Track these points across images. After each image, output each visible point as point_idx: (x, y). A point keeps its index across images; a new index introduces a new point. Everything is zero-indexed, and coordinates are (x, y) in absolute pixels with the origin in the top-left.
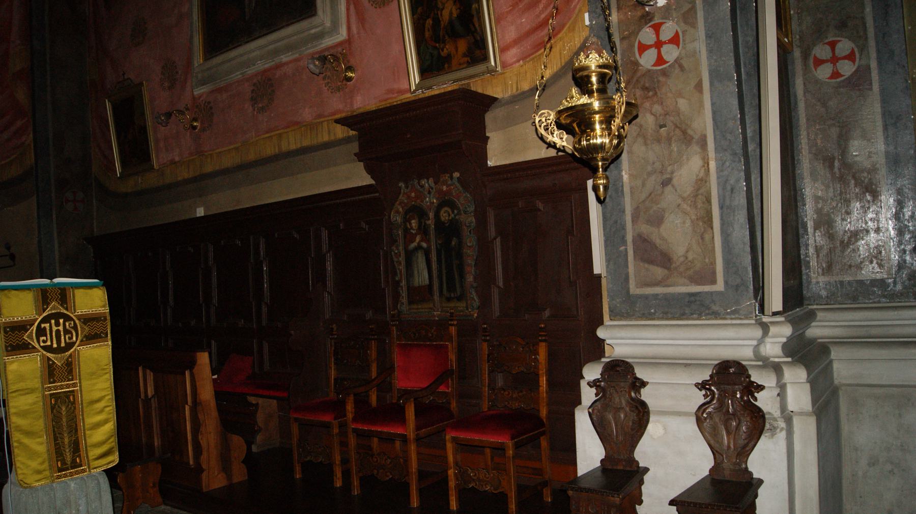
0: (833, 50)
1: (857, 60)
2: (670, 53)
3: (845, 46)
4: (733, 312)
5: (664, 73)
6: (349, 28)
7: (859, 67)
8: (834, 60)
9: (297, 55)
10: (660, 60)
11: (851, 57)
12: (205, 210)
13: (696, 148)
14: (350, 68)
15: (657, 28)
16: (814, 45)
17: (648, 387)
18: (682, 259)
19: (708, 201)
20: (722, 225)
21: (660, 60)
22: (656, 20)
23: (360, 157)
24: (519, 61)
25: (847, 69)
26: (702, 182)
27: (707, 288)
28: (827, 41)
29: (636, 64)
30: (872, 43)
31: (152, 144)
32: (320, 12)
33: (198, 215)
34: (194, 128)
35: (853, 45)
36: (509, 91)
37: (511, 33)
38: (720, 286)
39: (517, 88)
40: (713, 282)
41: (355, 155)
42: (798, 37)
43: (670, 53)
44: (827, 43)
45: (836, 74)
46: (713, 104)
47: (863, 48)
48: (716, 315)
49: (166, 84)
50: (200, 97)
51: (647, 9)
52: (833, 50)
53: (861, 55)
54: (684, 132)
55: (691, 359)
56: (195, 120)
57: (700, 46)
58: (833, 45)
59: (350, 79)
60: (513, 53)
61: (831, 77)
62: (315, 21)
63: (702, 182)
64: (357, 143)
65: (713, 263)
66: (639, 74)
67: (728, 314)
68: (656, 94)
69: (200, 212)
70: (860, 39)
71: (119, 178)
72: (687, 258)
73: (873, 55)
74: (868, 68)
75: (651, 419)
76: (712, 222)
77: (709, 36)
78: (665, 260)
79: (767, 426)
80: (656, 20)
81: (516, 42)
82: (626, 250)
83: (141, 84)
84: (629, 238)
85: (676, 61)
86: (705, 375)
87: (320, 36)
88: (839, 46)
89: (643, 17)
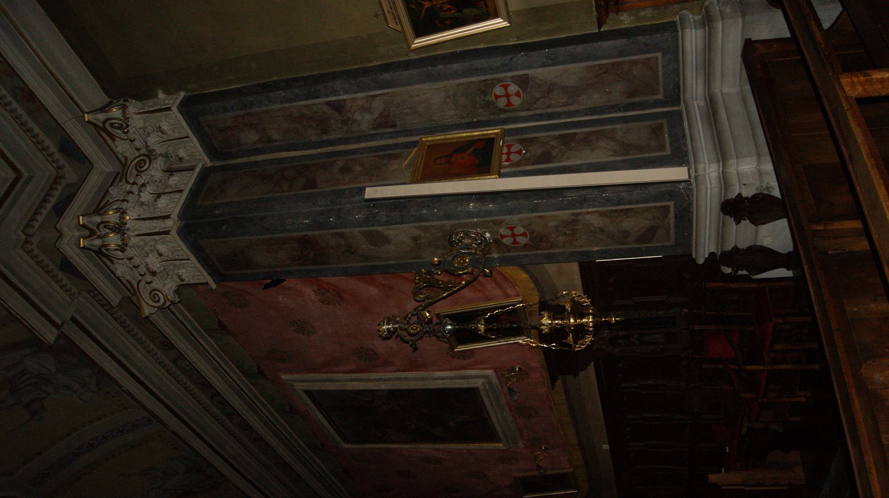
0: (500, 97)
1: (508, 83)
2: (519, 230)
3: (498, 90)
4: (688, 196)
5: (531, 233)
6: (487, 369)
7: (512, 82)
8: (507, 96)
9: (502, 395)
10: (524, 235)
11: (506, 87)
12: (605, 444)
13: (580, 217)
14: (513, 370)
15: (503, 237)
16: (497, 107)
17: (738, 245)
18: (652, 222)
19: (612, 211)
20: (630, 204)
21: (524, 235)
22: (499, 237)
23: (576, 375)
24: (515, 289)
25: (513, 88)
26: (602, 214)
27: (672, 210)
28: (495, 101)
29: (525, 245)
30: (496, 76)
31: (556, 472)
32: (476, 385)
33: (609, 448)
34: (546, 448)
35: (497, 86)
36: (534, 293)
37: (498, 292)
38: (671, 204)
39: (533, 289)
40: (668, 207)
41: (575, 377)
42: (492, 116)
43: (519, 230)
44: (496, 100)
45: (518, 94)
46: (553, 211)
47: (499, 80)
48: (690, 205)
49: (515, 462)
50: (525, 444)
51: (491, 241)
52: (500, 97)
53: (504, 82)
54: (570, 223)
55: (715, 145)
56: (541, 448)
57: (515, 218)
58: (497, 97)
59: (520, 369)
60: (509, 291)
61: (520, 97)
62: (481, 388)
63: (602, 214)
64: (567, 376)
65: (656, 207)
66: (532, 244)
67: (689, 199)
68: (545, 236)
69: (606, 447)
70: (493, 83)
71: (578, 491)
72: (651, 219)
73: (504, 75)
74: (512, 77)
75: (760, 244)
76: (629, 209)
77: (510, 214)
78: (653, 230)
79: (766, 192)
80: (499, 237)
81: (504, 291)
82: (644, 247)
83: (515, 478)
84: (636, 246)
85: (524, 228)
86: (731, 221)
87: (491, 384)
88: (498, 93)
89: (496, 243)
